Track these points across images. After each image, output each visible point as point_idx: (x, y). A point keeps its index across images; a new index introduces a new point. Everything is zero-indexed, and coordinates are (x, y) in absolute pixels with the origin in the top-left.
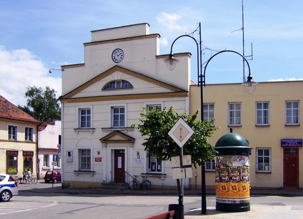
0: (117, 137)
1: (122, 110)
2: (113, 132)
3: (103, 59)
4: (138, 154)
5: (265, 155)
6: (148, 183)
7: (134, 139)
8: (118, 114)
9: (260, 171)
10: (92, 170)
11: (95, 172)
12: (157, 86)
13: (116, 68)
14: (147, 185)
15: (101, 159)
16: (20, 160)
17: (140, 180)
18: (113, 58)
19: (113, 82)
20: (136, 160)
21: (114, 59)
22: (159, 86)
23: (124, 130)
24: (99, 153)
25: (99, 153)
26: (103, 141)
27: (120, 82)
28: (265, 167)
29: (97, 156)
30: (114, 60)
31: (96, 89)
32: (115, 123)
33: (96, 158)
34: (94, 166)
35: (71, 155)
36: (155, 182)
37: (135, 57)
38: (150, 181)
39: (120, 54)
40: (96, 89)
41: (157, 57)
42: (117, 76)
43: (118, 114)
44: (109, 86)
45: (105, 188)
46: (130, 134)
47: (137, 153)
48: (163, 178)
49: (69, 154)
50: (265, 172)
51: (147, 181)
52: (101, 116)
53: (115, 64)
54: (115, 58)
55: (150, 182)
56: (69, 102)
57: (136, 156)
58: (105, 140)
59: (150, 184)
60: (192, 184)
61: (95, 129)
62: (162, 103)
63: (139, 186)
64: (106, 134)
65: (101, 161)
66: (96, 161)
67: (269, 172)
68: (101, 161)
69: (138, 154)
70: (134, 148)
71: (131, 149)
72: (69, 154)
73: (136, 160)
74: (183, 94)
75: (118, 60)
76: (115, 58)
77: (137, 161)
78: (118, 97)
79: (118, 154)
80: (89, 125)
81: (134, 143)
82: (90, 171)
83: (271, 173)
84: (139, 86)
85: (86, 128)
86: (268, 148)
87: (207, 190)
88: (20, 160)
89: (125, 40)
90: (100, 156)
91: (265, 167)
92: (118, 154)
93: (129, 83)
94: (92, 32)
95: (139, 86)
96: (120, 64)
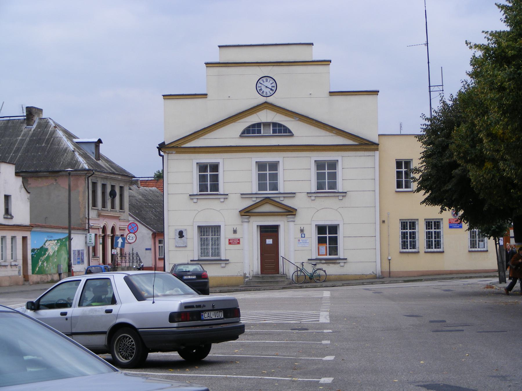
0: (267, 208)
1: (215, 167)
2: (261, 201)
3: (241, 91)
4: (302, 231)
5: (407, 232)
6: (322, 273)
7: (296, 210)
8: (268, 173)
9: (473, 249)
10: (223, 258)
11: (228, 260)
12: (331, 134)
13: (266, 105)
14: (319, 276)
15: (239, 240)
16: (421, 231)
17: (309, 269)
18: (258, 89)
19: (259, 125)
20: (299, 241)
21: (259, 91)
22: (333, 134)
23: (279, 197)
24: (235, 232)
25: (235, 232)
26: (245, 213)
27: (270, 125)
28: (479, 243)
29: (233, 236)
30: (261, 93)
31: (231, 135)
32: (262, 187)
33: (229, 240)
34: (226, 250)
35: (183, 236)
36: (332, 270)
37: (296, 91)
38: (324, 269)
39: (262, 86)
40: (231, 135)
41: (332, 94)
42: (265, 116)
43: (268, 173)
44: (253, 130)
45: (261, 282)
46: (288, 202)
47: (234, 230)
48: (342, 264)
49: (181, 234)
50: (479, 249)
51: (318, 269)
52: (239, 176)
53: (262, 100)
54: (261, 90)
55: (325, 271)
56: (178, 152)
57: (299, 235)
58: (247, 213)
59: (324, 274)
60: (384, 270)
61: (295, 193)
62: (340, 159)
63: (308, 277)
64: (247, 203)
65: (239, 243)
66: (230, 243)
67: (485, 249)
68: (239, 243)
69: (302, 231)
70: (296, 223)
71: (292, 224)
72: (181, 234)
73: (299, 241)
74: (373, 147)
75: (266, 93)
76: (261, 90)
77: (301, 241)
78: (302, 148)
79: (269, 232)
80: (333, 185)
81: (295, 215)
82: (221, 260)
83: (487, 251)
84: (303, 134)
85: (209, 193)
86: (439, 219)
87: (42, 305)
88: (421, 231)
89: (278, 64)
90: (236, 236)
91: (479, 243)
92: (269, 232)
93: (284, 126)
94: (219, 46)
95: (303, 134)
96: (270, 100)
